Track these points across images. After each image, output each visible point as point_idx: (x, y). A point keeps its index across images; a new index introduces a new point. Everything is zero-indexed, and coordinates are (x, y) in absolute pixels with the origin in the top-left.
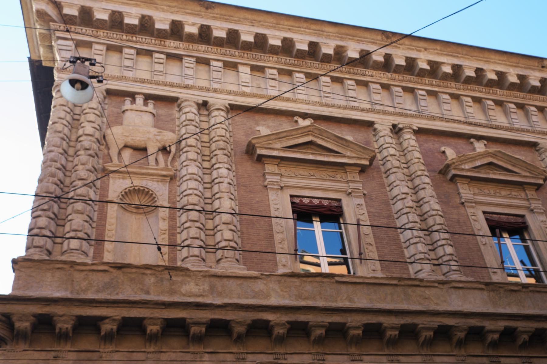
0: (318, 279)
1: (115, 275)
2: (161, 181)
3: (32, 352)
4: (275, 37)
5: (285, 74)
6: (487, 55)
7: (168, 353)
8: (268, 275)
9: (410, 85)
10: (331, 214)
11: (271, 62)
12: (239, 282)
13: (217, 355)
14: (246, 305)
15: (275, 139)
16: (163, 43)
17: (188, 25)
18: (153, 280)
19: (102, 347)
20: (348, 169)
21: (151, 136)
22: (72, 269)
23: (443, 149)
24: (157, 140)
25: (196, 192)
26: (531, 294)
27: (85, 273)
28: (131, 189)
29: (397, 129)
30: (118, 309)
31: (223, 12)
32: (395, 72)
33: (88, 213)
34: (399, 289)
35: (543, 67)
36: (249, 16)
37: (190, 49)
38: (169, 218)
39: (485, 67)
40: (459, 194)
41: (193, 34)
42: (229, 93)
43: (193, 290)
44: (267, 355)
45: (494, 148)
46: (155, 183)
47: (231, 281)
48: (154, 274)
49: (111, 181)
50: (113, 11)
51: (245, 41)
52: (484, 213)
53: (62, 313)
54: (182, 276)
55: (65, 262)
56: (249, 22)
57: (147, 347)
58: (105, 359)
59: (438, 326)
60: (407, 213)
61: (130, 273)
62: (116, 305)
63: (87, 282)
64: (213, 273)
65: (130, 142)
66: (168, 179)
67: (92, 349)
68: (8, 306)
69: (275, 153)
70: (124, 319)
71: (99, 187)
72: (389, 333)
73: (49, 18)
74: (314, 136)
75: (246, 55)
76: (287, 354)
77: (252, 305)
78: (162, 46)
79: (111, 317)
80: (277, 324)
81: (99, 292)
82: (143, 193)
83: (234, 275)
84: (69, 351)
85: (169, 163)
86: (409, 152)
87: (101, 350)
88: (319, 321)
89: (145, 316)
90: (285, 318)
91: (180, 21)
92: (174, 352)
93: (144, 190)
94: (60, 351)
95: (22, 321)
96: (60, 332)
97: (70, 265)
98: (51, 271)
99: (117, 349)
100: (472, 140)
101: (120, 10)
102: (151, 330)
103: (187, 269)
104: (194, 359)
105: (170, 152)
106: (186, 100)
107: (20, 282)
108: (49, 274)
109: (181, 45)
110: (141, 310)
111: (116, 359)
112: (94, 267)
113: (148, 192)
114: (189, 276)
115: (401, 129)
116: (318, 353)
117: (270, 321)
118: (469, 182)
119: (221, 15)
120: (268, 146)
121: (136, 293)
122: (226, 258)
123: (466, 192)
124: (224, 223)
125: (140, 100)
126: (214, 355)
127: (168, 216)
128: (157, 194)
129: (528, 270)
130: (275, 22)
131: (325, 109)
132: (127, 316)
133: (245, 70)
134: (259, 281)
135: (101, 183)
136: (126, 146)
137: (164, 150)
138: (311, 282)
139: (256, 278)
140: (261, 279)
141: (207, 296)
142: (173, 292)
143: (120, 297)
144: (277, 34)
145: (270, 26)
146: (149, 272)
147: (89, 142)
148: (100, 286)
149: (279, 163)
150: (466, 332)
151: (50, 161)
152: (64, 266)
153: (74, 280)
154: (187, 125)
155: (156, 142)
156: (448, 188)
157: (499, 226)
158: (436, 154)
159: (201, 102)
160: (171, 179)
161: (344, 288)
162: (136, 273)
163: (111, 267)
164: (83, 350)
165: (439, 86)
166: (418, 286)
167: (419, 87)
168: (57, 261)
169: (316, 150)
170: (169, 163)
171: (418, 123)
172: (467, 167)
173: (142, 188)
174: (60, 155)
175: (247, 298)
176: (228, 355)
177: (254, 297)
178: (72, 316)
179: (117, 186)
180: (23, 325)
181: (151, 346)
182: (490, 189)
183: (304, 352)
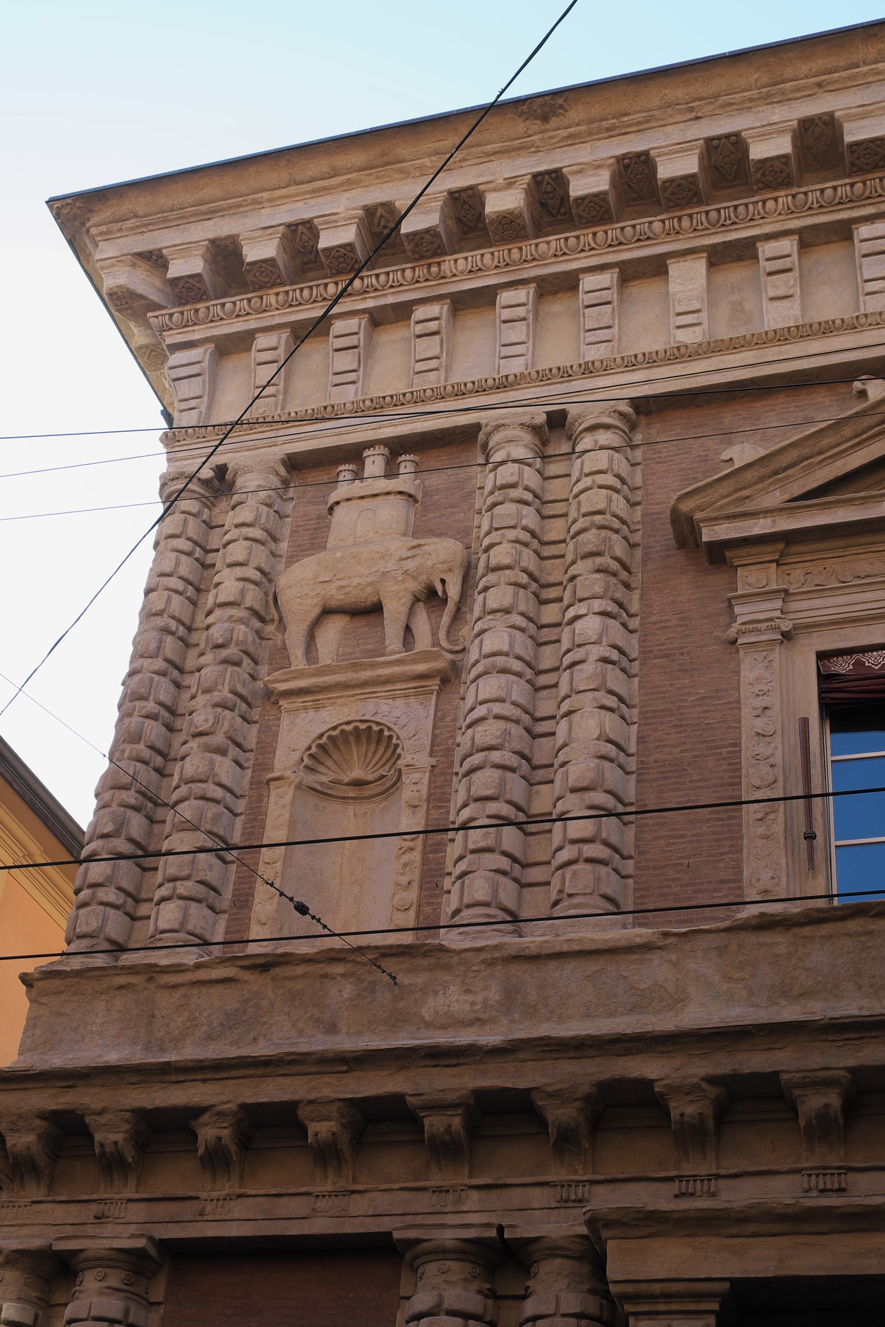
0: (854, 925)
1: (255, 988)
3: (51, 1206)
4: (768, 132)
5: (828, 242)
7: (369, 1195)
8: (685, 934)
11: (771, 218)
12: (592, 966)
13: (505, 1193)
14: (573, 1038)
15: (761, 479)
16: (434, 269)
17: (495, 190)
18: (348, 989)
21: (391, 565)
22: (151, 986)
24: (405, 572)
25: (497, 708)
27: (182, 991)
28: (334, 733)
30: (231, 1082)
31: (596, 111)
33: (208, 827)
36: (677, 92)
37: (515, 263)
38: (428, 801)
41: (511, 213)
43: (455, 1007)
44: (655, 1185)
46: (400, 702)
47: (571, 965)
48: (353, 974)
49: (285, 721)
50: (289, 226)
51: (672, 180)
53: (99, 1106)
56: (680, 112)
58: (210, 1218)
62: (223, 1075)
63: (185, 1014)
64: (513, 951)
65: (336, 596)
66: (434, 684)
67: (180, 1193)
71: (253, 746)
73: (143, 302)
75: (686, 223)
76: (718, 1177)
77: (590, 1037)
78: (435, 279)
79: (213, 1106)
80: (676, 1089)
81: (212, 1039)
82: (347, 741)
83: (576, 948)
84: (130, 1200)
87: (203, 1195)
88: (814, 1066)
89: (296, 1097)
90: (697, 1068)
91: (471, 188)
92: (385, 1190)
93: (370, 728)
95: (18, 1130)
96: (103, 1153)
97: (146, 976)
98: (103, 997)
101: (307, 215)
102: (316, 1134)
104: (438, 1208)
105: (444, 601)
106: (498, 427)
107: (38, 1032)
108: (100, 1006)
109: (487, 256)
111: (236, 1215)
112: (202, 975)
113: (381, 731)
114: (448, 968)
116: (823, 1170)
117: (652, 1082)
119: (590, 121)
120: (740, 509)
121: (301, 1032)
122: (570, 896)
124: (574, 790)
125: (374, 463)
126: (495, 1193)
127: (425, 796)
130: (765, 80)
132: (252, 1101)
133: (688, 279)
134: (656, 958)
135: (259, 731)
136: (327, 612)
137: (431, 597)
138: (830, 936)
139: (646, 947)
140: (660, 948)
141: (492, 1021)
142: (398, 1020)
143: (262, 1050)
144: (775, 118)
145: (751, 100)
146: (338, 969)
147: (226, 625)
148: (215, 1024)
149: (782, 554)
151: (131, 701)
153: (156, 1012)
154: (495, 505)
155: (403, 581)
159: (541, 419)
160: (445, 682)
162: (304, 976)
164: (160, 1195)
170: (442, 635)
173: (363, 726)
174: (156, 678)
175: (612, 1014)
176: (537, 1191)
177: (634, 1009)
178: (121, 1111)
179: (299, 730)
180: (111, 1135)
181: (326, 1177)
183: (775, 1168)
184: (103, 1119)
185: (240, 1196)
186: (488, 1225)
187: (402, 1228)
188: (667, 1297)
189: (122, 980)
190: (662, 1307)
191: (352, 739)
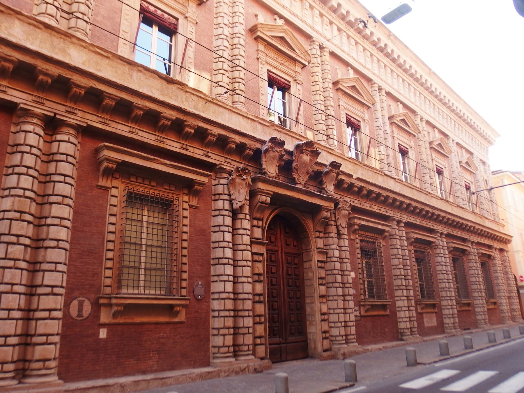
10: (284, 88)
20: (298, 64)
59: (176, 118)
72: (163, 121)
100: (276, 17)
157: (273, 82)
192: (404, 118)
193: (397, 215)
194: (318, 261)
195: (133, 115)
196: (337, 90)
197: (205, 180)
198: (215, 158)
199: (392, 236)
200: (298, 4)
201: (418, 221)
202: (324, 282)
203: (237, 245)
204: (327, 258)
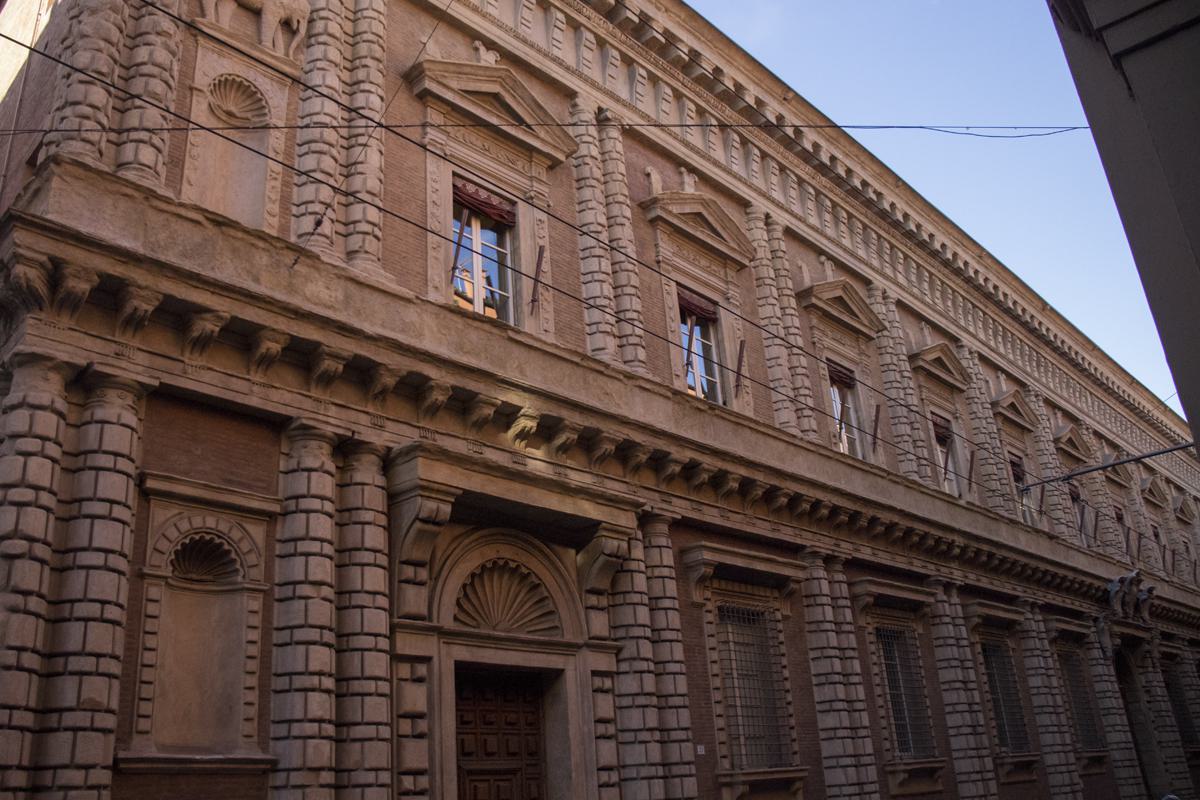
2: (278, 82)
6: (733, 53)
9: (631, 54)
10: (501, 224)
15: (454, 72)
19: (187, 354)
22: (146, 203)
23: (649, 169)
26: (715, 420)
27: (165, 216)
29: (602, 116)
32: (620, 26)
34: (579, 371)
35: (785, 99)
39: (726, 69)
40: (656, 246)
42: (792, 213)
43: (322, 295)
45: (708, 194)
47: (376, 295)
52: (455, 174)
53: (144, 284)
54: (308, 266)
55: (138, 187)
57: (252, 373)
60: (599, 256)
61: (234, 238)
64: (352, 276)
68: (62, 246)
69: (449, 96)
70: (234, 319)
74: (504, 87)
77: (414, 348)
80: (439, 387)
84: (139, 349)
85: (291, 52)
86: (612, 159)
87: (186, 361)
89: (267, 324)
94: (127, 346)
99: (210, 366)
100: (478, 43)
103: (318, 258)
110: (261, 312)
114: (317, 269)
115: (608, 119)
117: (431, 379)
118: (448, 113)
122: (366, 252)
123: (667, 248)
126: (343, 410)
128: (270, 102)
129: (492, 292)
131: (520, 45)
139: (409, 301)
146: (261, 244)
150: (648, 455)
152: (136, 194)
156: (646, 231)
157: (467, 207)
158: (639, 175)
161: (517, 350)
162: (242, 239)
163: (207, 219)
165: (664, 70)
166: (601, 373)
167: (641, 61)
168: (126, 181)
169: (497, 109)
171: (630, 118)
172: (675, 209)
173: (246, 84)
181: (134, 336)
182: (689, 250)
184: (142, 293)
185: (209, 369)
186: (349, 429)
187: (101, 364)
188: (438, 491)
189: (129, 191)
190: (434, 495)
191: (235, 86)
192: (839, 293)
193: (824, 544)
194: (595, 673)
195: (258, 354)
196: (806, 308)
197: (801, 575)
198: (280, 395)
199: (1025, 634)
200: (532, 15)
201: (1057, 600)
202: (611, 729)
203: (348, 635)
204: (618, 661)
